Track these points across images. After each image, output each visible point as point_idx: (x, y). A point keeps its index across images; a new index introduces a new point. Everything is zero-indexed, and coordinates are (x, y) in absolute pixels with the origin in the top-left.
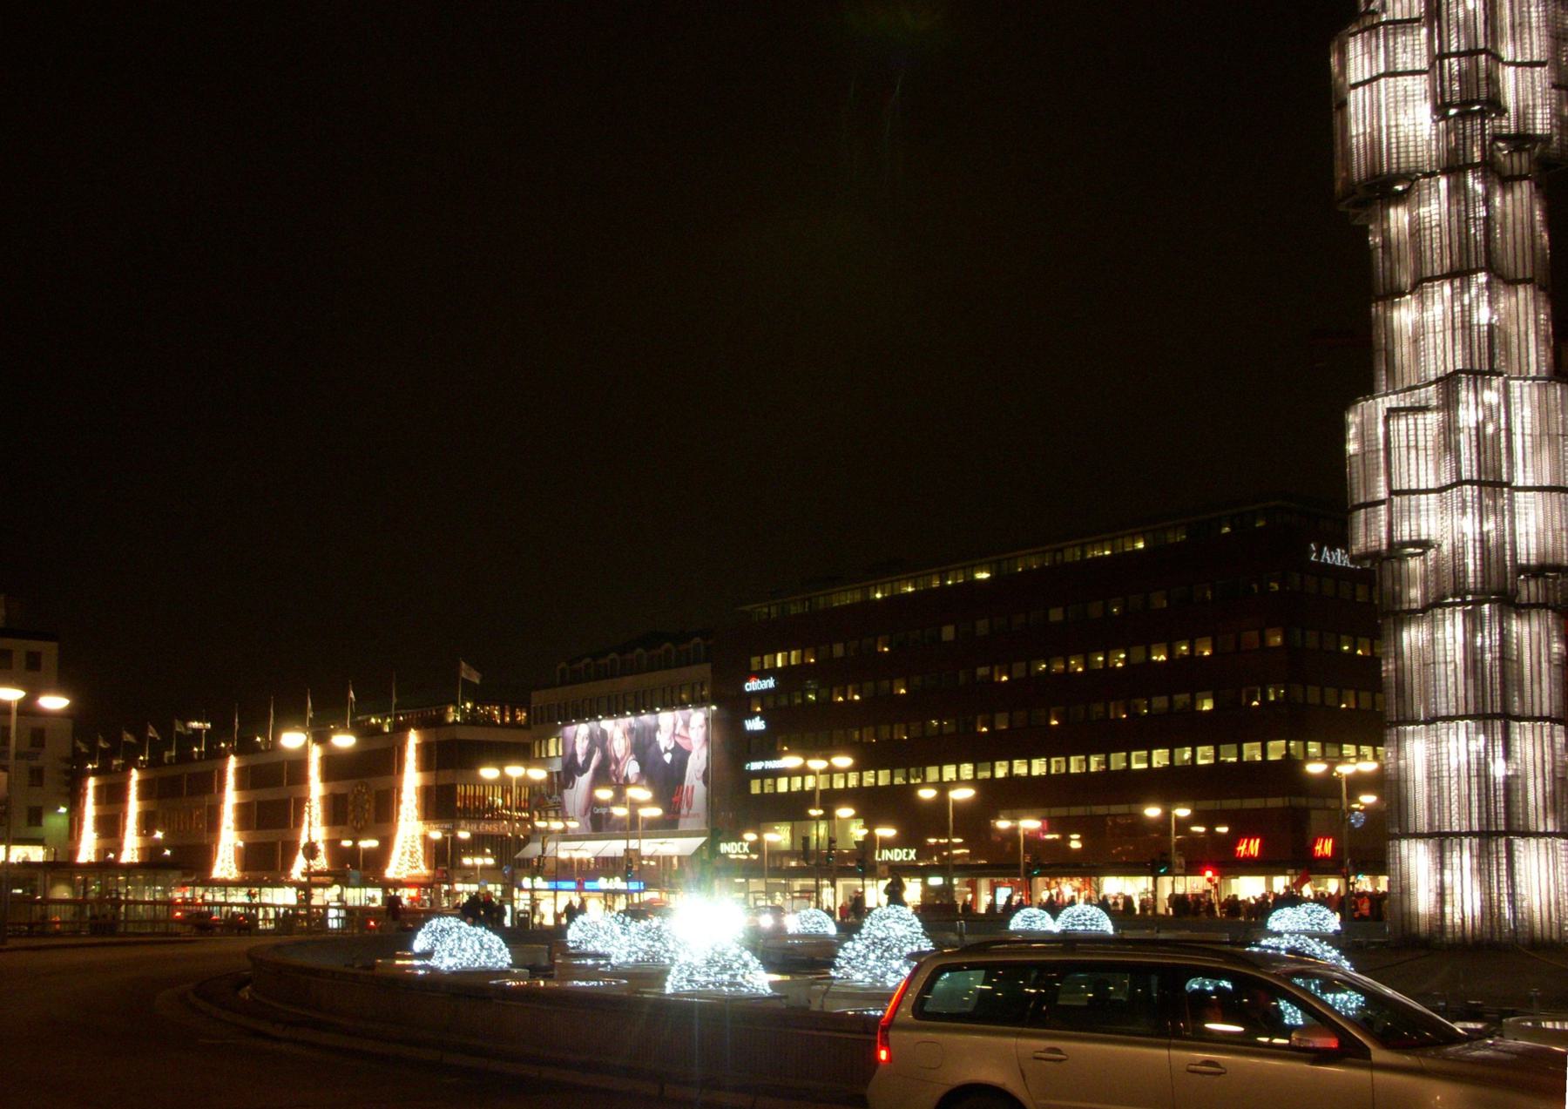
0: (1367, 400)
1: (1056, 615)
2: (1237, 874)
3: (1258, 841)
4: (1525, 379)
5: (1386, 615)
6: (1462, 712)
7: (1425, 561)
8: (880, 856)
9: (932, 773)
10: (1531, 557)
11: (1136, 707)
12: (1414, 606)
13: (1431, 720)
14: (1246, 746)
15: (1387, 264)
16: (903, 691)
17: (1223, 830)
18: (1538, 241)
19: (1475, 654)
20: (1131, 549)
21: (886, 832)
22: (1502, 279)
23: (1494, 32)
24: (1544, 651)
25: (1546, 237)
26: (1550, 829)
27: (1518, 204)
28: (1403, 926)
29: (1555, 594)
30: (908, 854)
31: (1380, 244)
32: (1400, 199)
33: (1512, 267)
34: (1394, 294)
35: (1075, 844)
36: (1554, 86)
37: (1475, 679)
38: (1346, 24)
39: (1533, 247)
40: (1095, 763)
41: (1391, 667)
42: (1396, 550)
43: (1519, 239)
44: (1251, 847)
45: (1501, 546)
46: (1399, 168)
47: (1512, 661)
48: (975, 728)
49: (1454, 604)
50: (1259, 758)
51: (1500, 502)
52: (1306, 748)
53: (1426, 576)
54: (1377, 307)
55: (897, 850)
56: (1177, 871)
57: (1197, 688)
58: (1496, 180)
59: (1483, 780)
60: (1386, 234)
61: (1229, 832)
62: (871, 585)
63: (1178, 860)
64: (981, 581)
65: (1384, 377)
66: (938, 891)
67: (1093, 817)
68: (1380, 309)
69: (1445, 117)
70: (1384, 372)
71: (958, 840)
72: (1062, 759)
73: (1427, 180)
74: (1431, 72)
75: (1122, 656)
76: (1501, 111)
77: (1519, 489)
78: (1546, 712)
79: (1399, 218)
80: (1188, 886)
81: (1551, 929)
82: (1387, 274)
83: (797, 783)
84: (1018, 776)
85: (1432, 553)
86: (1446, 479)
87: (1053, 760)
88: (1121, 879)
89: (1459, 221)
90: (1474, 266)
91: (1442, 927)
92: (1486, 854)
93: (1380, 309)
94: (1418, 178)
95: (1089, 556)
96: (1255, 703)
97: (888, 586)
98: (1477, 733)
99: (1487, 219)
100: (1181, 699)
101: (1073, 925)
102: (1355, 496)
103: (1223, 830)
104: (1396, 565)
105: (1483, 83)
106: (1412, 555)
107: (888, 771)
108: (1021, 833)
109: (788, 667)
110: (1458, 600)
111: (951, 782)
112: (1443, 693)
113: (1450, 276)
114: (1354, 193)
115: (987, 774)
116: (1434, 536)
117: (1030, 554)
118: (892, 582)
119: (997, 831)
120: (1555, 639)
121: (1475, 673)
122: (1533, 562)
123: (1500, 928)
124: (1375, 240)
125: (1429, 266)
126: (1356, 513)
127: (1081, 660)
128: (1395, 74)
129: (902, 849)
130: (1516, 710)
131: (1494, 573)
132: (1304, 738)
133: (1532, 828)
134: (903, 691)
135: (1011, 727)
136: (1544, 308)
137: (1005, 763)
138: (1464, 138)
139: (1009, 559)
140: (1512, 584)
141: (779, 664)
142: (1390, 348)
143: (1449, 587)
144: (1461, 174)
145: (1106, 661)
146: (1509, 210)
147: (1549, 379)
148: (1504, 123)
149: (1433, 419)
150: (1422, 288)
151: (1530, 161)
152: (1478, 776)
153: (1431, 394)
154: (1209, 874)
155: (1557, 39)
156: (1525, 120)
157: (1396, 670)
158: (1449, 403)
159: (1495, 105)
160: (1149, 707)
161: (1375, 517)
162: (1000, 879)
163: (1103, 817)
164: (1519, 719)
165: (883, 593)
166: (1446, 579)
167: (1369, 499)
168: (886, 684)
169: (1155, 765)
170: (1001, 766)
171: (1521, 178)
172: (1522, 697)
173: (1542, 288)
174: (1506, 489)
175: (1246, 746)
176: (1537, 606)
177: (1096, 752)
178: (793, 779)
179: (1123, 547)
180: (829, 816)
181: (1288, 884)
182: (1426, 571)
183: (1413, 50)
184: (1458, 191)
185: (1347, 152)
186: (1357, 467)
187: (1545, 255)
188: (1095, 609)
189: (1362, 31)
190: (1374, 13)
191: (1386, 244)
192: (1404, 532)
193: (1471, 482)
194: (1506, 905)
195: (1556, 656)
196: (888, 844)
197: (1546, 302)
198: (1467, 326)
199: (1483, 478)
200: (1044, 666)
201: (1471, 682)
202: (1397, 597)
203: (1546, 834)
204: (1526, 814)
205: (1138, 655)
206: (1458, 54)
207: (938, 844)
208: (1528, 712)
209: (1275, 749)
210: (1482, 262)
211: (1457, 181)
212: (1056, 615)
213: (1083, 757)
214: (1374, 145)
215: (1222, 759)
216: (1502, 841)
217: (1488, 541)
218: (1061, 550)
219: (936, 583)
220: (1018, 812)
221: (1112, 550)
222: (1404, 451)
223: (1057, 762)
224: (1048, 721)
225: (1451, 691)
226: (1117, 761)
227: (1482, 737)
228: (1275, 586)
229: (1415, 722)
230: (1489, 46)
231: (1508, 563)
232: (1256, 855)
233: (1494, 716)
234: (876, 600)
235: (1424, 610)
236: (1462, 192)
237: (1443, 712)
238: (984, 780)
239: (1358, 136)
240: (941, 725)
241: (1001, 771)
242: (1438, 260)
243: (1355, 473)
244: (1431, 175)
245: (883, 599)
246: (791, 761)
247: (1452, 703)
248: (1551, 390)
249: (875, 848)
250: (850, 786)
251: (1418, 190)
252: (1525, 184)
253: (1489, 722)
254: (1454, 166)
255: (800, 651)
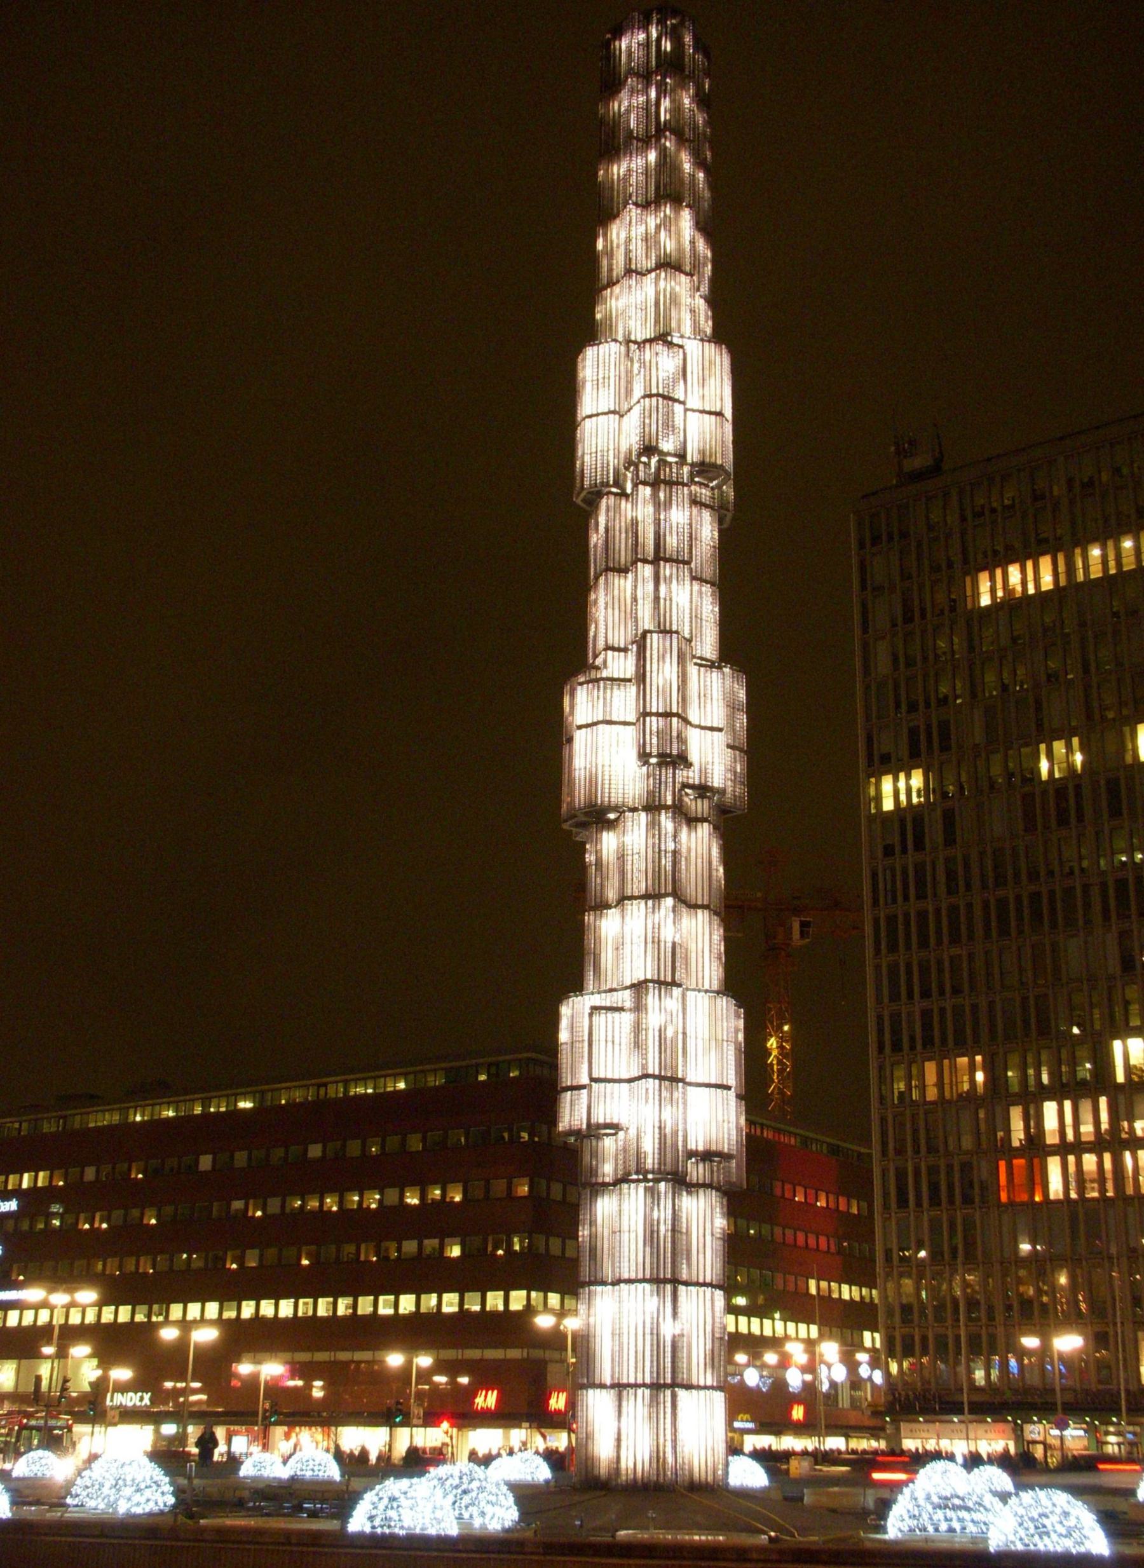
0: (577, 996)
1: (315, 1151)
2: (475, 1426)
3: (495, 1392)
4: (699, 991)
5: (586, 1185)
6: (640, 1276)
7: (616, 1140)
8: (112, 1400)
9: (176, 1311)
10: (699, 1144)
11: (387, 1249)
12: (607, 1180)
13: (617, 1282)
14: (489, 1295)
15: (599, 880)
16: (153, 1221)
17: (464, 1380)
18: (714, 873)
19: (652, 1225)
20: (392, 1089)
21: (122, 1374)
22: (684, 902)
23: (684, 699)
24: (708, 1225)
25: (721, 870)
26: (709, 1383)
27: (700, 841)
28: (587, 1467)
29: (718, 1177)
30: (142, 1399)
31: (594, 862)
32: (611, 825)
33: (694, 893)
34: (603, 906)
35: (318, 1393)
36: (729, 746)
37: (652, 1247)
38: (575, 673)
39: (710, 876)
40: (343, 1306)
41: (586, 1233)
42: (594, 1131)
43: (699, 871)
44: (487, 1400)
45: (675, 1133)
46: (610, 801)
47: (681, 1233)
48: (225, 1265)
49: (638, 1181)
50: (501, 1308)
51: (675, 1095)
52: (546, 1298)
53: (617, 1155)
54: (589, 915)
55: (131, 1394)
56: (415, 1421)
57: (445, 1235)
58: (684, 821)
59: (655, 1337)
60: (599, 855)
61: (469, 1383)
62: (131, 1107)
63: (417, 1411)
64: (244, 1110)
65: (592, 978)
66: (171, 1439)
67: (335, 1363)
68: (592, 918)
69: (646, 763)
70: (592, 973)
71: (196, 1385)
72: (310, 1301)
73: (631, 814)
74: (637, 724)
75: (378, 1197)
76: (689, 765)
77: (690, 1084)
78: (708, 1280)
79: (609, 842)
80: (428, 1440)
81: (707, 1472)
82: (599, 888)
83: (28, 1318)
84: (264, 1317)
85: (621, 1134)
86: (636, 1073)
87: (301, 1301)
88: (361, 1429)
89: (653, 852)
90: (663, 891)
91: (618, 1469)
92: (655, 1404)
93: (592, 918)
94: (624, 812)
95: (352, 1093)
96: (500, 1252)
97: (148, 1110)
98: (652, 1295)
99: (675, 852)
100: (431, 1244)
101: (302, 1470)
102: (564, 1080)
103: (464, 1380)
104: (594, 1143)
105: (675, 741)
106: (607, 1135)
107: (130, 1307)
108: (262, 1378)
109: (34, 1189)
110: (641, 1177)
111: (195, 1321)
112: (626, 1259)
113: (646, 897)
114: (575, 816)
115: (232, 1314)
116: (624, 1122)
117: (295, 1087)
118: (153, 1105)
119: (237, 1376)
120: (718, 1215)
121: (652, 1242)
122: (701, 1148)
123: (664, 1469)
124: (590, 858)
125: (629, 886)
126: (563, 1095)
127: (337, 1199)
128: (610, 722)
129: (136, 1393)
130: (684, 1276)
131: (669, 1156)
132: (545, 1289)
133: (695, 1382)
134: (153, 1221)
135: (261, 1265)
136: (718, 930)
137: (253, 1303)
138: (660, 783)
139: (272, 1090)
140: (683, 1166)
141: (25, 1185)
142: (597, 952)
143: (633, 1167)
144: (657, 813)
145: (360, 1202)
146: (693, 846)
147: (718, 992)
148: (691, 774)
149: (627, 1018)
150: (623, 905)
151: (710, 808)
152: (652, 1334)
153: (625, 998)
154: (445, 1425)
155: (733, 708)
156: (706, 773)
157: (590, 1236)
158: (639, 1007)
159: (681, 760)
160: (399, 1250)
161: (578, 1099)
162: (237, 1428)
163: (347, 1363)
164: (687, 1284)
165: (143, 1115)
166: (631, 1158)
167: (575, 1083)
168: (135, 1212)
169: (401, 1311)
170: (248, 1305)
171: (703, 820)
172: (689, 1265)
173: (716, 913)
174: (680, 1085)
175: (489, 1295)
176: (704, 1186)
177: (344, 1294)
178: (25, 1312)
179: (385, 1087)
180: (62, 1354)
181: (524, 1439)
182: (617, 1150)
183: (624, 702)
184: (654, 825)
185: (571, 781)
186: (567, 1054)
187: (720, 886)
188: (354, 1148)
189: (588, 682)
190: (598, 668)
191: (599, 863)
192: (599, 1117)
193: (654, 1076)
194: (669, 1450)
195: (719, 1230)
196: (122, 1388)
197: (719, 925)
198: (657, 942)
199: (663, 1074)
200: (299, 1203)
201: (648, 1249)
202: (594, 1172)
203: (706, 1388)
204: (690, 1370)
205: (392, 1195)
206: (658, 715)
207: (174, 1388)
208: (694, 1279)
209: (518, 1299)
210: (670, 889)
211: (654, 819)
212: (315, 1151)
213: (331, 1299)
214: (592, 781)
215: (466, 1307)
216: (668, 1392)
217: (665, 1127)
218: (325, 1085)
219: (198, 1110)
220: (259, 1356)
221: (374, 1089)
222: (603, 1043)
223: (306, 1304)
224: (300, 1260)
225: (633, 1257)
226: (365, 1305)
227: (655, 1297)
228: (525, 1136)
229: (603, 1283)
230: (680, 712)
231: (680, 1148)
232: (493, 1408)
233: (665, 1281)
234: (135, 1123)
235: (614, 1184)
236: (657, 827)
237: (626, 1276)
238: (229, 1320)
239: (580, 769)
240: (190, 1257)
241: (248, 1310)
242: (638, 885)
243: (565, 1058)
244: (634, 810)
245: (143, 1123)
246: (33, 1294)
247: (633, 1268)
248: (719, 1000)
249: (108, 1391)
250: (87, 1321)
251: (624, 822)
252: (706, 825)
253: (662, 1286)
254: (652, 807)
255: (48, 1172)
